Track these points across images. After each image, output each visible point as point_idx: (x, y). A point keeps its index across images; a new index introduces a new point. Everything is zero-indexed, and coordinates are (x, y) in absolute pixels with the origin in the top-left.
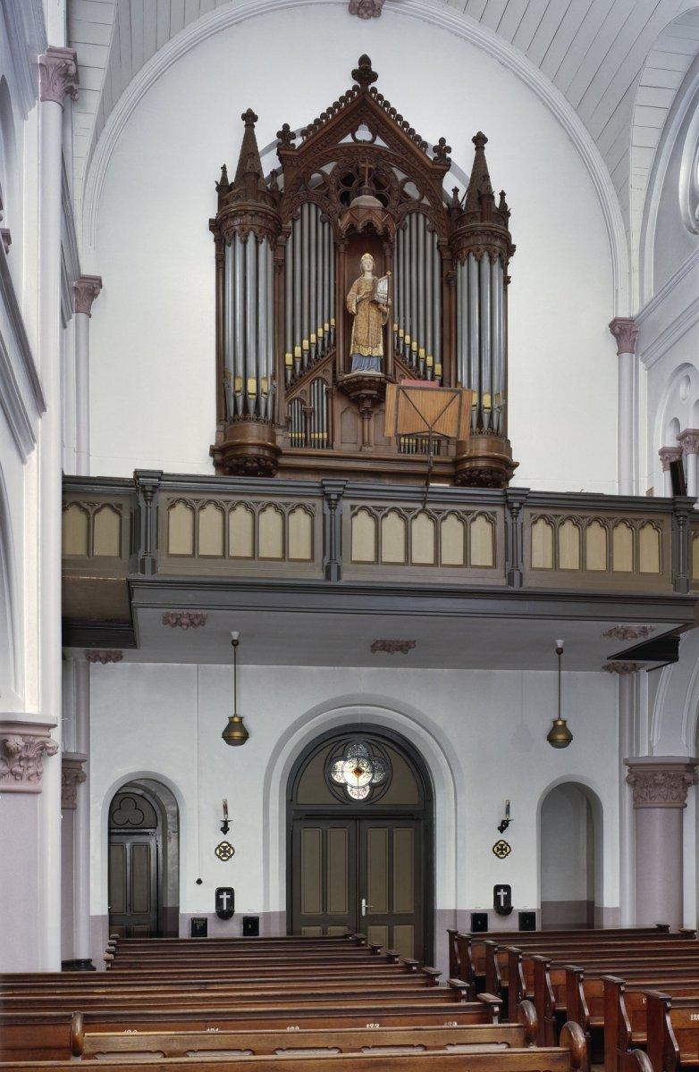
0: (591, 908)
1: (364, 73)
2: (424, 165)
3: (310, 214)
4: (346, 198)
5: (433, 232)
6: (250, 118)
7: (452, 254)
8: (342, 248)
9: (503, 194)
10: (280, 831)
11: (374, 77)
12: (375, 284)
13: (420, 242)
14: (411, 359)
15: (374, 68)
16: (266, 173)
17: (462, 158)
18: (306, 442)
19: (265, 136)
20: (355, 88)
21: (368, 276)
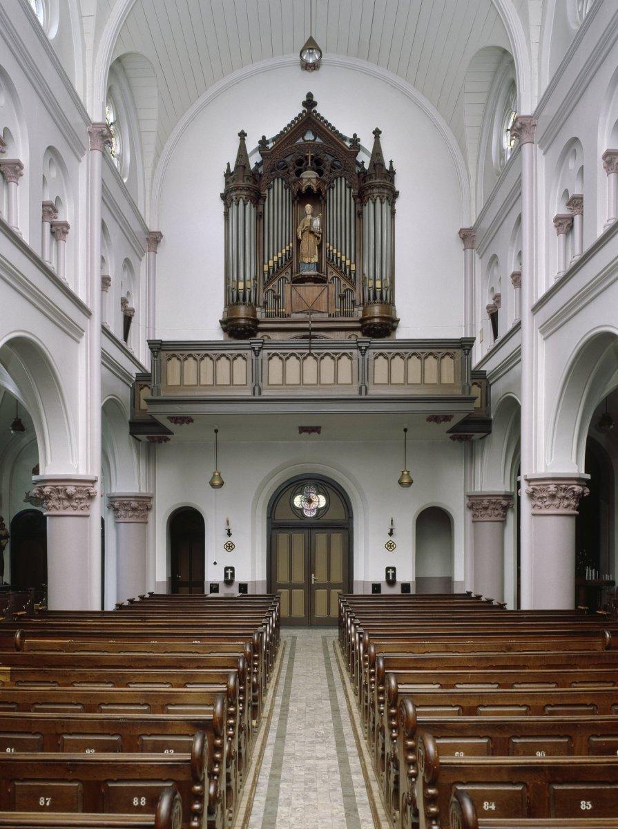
0: (449, 581)
1: (310, 103)
2: (344, 150)
3: (278, 185)
4: (298, 173)
5: (350, 188)
6: (243, 135)
7: (361, 197)
8: (296, 202)
9: (391, 162)
10: (514, 546)
11: (315, 104)
12: (311, 221)
13: (341, 194)
14: (337, 262)
15: (314, 99)
16: (252, 166)
17: (367, 143)
18: (277, 314)
19: (252, 144)
20: (304, 111)
21: (309, 217)
